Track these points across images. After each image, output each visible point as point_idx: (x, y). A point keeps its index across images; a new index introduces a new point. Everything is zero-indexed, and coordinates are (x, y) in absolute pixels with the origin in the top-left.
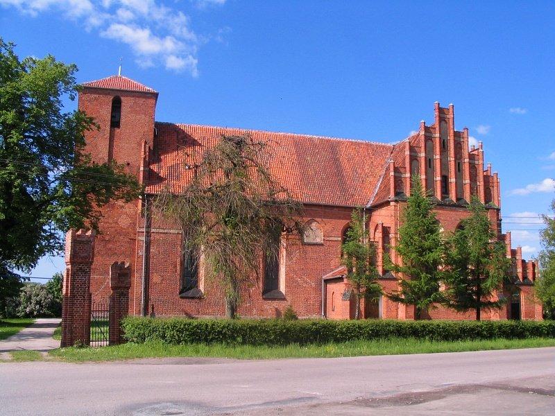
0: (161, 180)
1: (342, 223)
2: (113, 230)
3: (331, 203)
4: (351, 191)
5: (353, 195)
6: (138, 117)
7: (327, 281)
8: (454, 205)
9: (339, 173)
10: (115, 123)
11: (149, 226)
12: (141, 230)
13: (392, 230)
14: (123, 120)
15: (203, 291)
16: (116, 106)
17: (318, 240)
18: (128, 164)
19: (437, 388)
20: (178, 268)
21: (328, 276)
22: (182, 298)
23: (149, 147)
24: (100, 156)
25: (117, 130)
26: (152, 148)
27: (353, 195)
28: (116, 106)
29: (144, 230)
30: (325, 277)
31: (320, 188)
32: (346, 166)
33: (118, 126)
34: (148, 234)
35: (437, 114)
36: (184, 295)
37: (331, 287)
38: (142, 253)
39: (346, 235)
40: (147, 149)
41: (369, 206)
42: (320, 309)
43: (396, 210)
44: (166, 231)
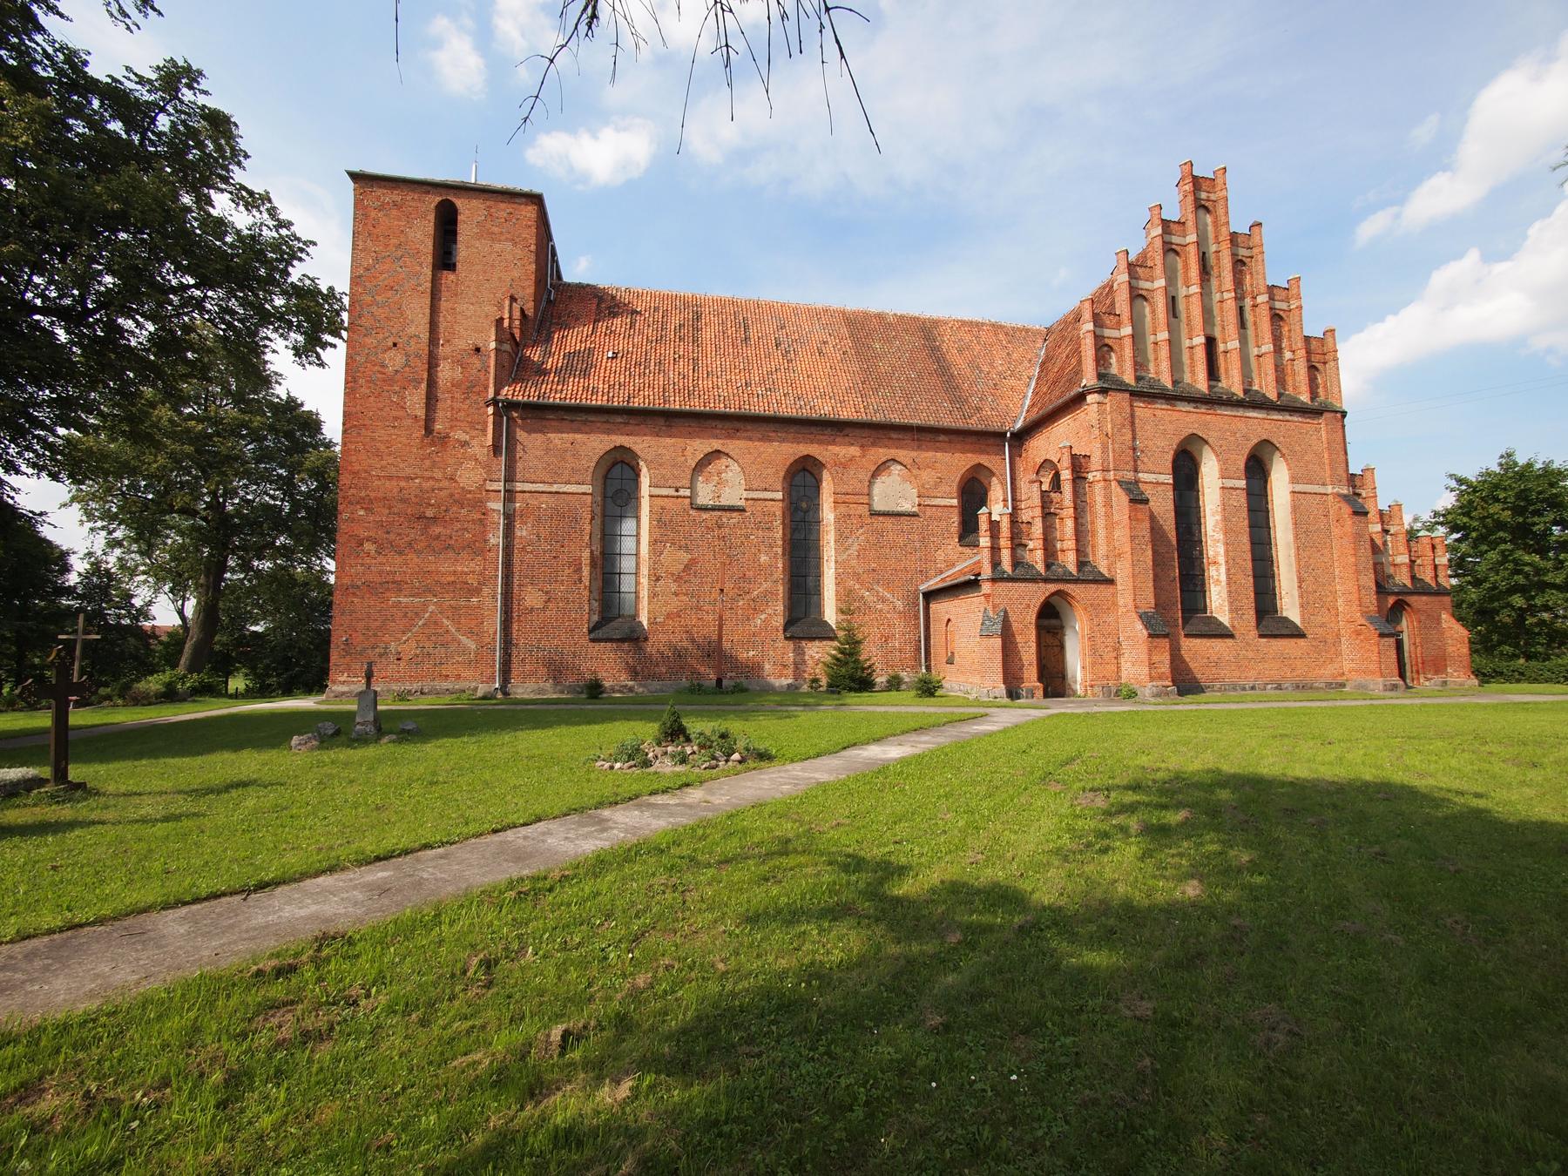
0: (542, 372)
1: (958, 462)
2: (443, 494)
3: (932, 422)
4: (975, 401)
5: (979, 409)
6: (497, 247)
7: (930, 596)
8: (1239, 404)
9: (943, 370)
10: (445, 259)
11: (510, 478)
12: (495, 486)
13: (1096, 462)
14: (462, 252)
15: (645, 623)
16: (447, 223)
17: (907, 507)
18: (478, 350)
19: (447, 699)
20: (586, 571)
21: (933, 583)
22: (593, 640)
23: (522, 311)
24: (411, 330)
25: (448, 277)
26: (530, 313)
27: (979, 409)
28: (447, 223)
29: (500, 486)
30: (923, 587)
31: (907, 397)
32: (959, 363)
33: (451, 267)
34: (510, 496)
35: (1159, 231)
36: (600, 634)
37: (940, 608)
38: (496, 539)
39: (973, 493)
40: (517, 314)
41: (1019, 425)
42: (917, 659)
43: (1100, 413)
44: (555, 488)
